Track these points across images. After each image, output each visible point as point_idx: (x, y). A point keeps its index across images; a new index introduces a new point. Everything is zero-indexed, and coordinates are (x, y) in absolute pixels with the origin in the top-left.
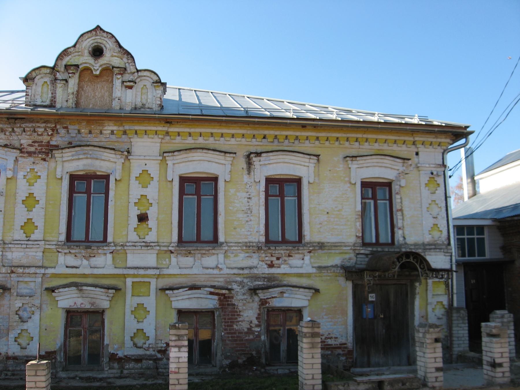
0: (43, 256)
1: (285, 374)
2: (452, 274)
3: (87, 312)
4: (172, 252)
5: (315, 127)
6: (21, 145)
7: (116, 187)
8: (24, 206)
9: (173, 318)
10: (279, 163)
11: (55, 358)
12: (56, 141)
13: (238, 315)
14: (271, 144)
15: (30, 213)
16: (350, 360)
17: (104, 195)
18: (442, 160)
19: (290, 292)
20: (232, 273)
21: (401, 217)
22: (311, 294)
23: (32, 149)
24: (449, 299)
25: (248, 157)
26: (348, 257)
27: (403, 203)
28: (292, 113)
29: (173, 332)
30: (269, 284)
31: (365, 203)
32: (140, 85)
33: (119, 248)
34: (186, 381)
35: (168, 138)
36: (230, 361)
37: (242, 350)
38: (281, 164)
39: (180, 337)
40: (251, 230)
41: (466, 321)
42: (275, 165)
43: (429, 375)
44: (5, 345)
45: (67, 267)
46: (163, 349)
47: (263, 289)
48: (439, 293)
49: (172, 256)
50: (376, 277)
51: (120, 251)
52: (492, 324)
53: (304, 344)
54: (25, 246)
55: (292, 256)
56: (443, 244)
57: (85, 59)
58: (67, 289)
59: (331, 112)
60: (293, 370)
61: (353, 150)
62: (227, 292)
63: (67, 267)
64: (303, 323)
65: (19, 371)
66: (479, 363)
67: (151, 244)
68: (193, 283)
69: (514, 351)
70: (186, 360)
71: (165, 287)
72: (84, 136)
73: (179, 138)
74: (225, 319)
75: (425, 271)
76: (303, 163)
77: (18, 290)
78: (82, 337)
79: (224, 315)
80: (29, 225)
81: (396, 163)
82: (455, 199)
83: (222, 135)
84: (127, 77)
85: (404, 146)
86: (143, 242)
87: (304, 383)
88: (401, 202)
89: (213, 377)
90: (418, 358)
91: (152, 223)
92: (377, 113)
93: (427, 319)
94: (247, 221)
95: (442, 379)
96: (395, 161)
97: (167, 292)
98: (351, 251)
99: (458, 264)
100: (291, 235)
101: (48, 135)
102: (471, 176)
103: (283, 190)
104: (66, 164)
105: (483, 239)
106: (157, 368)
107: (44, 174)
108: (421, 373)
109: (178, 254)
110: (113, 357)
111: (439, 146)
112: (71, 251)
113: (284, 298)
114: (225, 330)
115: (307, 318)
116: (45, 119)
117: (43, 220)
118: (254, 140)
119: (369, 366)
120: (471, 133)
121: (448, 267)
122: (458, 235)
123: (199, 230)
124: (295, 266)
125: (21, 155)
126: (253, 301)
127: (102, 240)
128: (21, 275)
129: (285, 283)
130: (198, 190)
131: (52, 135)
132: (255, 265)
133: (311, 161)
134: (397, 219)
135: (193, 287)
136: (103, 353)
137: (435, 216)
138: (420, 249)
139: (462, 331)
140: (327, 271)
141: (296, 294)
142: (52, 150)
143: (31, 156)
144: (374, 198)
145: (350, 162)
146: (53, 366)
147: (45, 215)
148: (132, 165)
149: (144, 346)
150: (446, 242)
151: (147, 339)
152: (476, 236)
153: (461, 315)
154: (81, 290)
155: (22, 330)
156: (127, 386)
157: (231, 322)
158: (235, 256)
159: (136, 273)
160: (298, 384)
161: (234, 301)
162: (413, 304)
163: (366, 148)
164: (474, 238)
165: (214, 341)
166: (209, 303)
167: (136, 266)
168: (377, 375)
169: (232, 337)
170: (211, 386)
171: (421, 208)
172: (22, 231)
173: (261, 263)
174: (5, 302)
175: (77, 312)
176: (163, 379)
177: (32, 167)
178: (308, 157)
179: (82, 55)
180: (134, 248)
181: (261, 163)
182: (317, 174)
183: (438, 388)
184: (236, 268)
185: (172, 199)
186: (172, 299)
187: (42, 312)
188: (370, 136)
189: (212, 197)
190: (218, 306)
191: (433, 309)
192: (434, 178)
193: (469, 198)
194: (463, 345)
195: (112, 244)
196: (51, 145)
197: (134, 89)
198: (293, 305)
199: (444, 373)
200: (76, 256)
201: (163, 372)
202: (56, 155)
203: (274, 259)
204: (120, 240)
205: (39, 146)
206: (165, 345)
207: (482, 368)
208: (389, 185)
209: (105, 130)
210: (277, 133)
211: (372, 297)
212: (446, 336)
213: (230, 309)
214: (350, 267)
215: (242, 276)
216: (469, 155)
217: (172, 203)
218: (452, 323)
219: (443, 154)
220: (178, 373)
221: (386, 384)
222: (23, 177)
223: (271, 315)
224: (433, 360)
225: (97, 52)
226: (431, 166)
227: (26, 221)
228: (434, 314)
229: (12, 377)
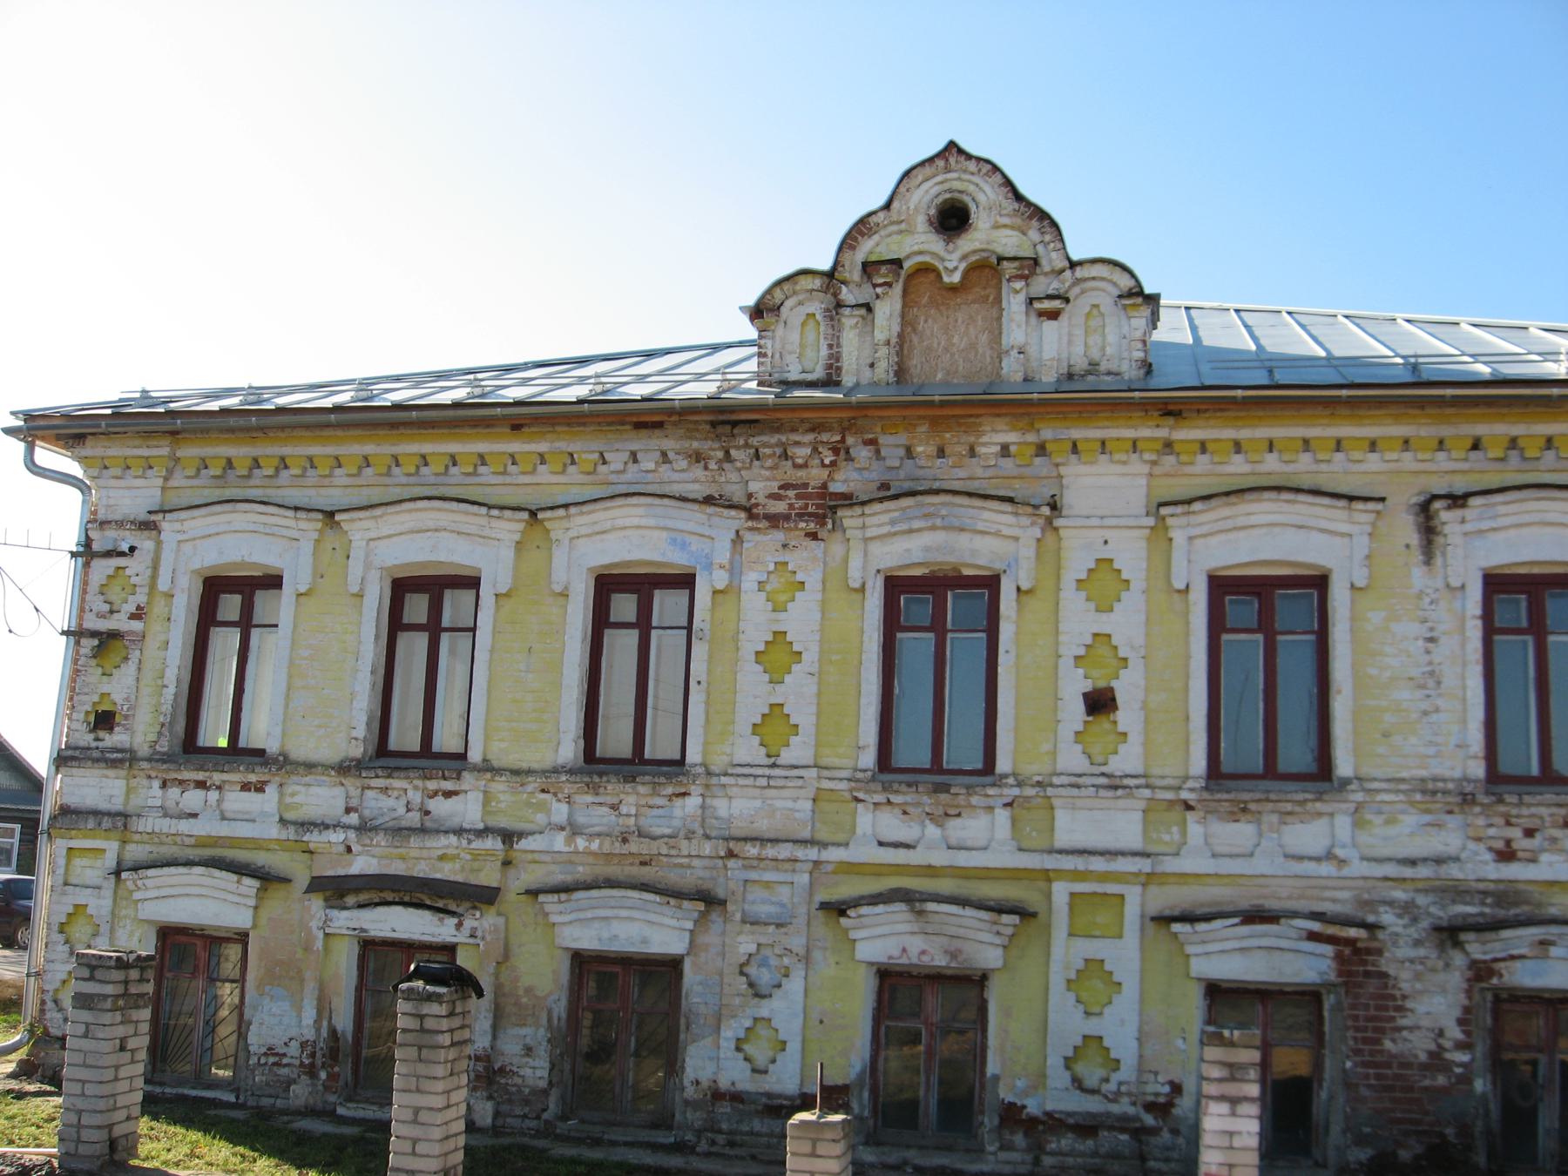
23: (780, 507)
30: (1501, 913)
49: (1190, 816)
51: (1033, 800)
57: (917, 241)
58: (880, 908)
84: (1041, 285)
91: (1127, 716)
97: (1177, 927)
104: (876, 549)
107: (813, 578)
110: (1011, 1115)
114: (1357, 1052)
116: (813, 419)
130: (1267, 614)
154: (921, 913)
161: (1386, 965)
181: (1468, 527)
186: (1190, 949)
197: (1064, 318)
203: (1516, 833)
204: (1034, 768)
210: (1517, 430)
217: (1188, 657)
225: (953, 218)
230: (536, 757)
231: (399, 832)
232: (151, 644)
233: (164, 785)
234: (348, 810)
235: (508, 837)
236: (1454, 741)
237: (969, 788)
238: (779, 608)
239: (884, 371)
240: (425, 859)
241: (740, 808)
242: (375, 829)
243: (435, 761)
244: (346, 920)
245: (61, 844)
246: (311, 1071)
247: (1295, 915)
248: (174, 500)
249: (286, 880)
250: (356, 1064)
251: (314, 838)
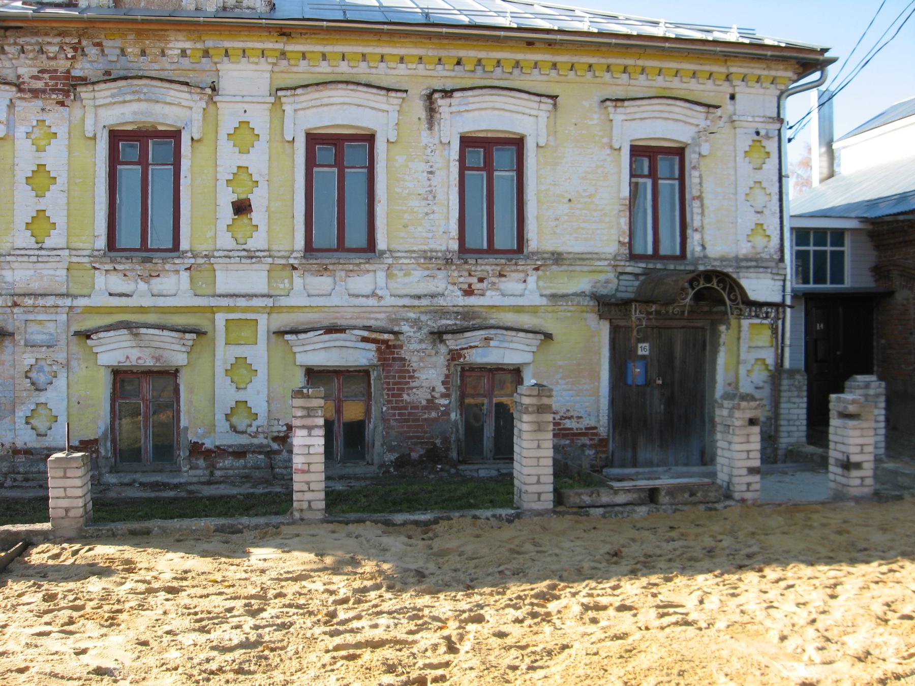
0: (67, 276)
1: (491, 477)
2: (784, 312)
3: (149, 373)
4: (294, 268)
5: (550, 44)
6: (19, 77)
7: (192, 152)
8: (30, 188)
9: (299, 380)
10: (486, 109)
11: (97, 451)
12: (81, 69)
13: (411, 377)
14: (471, 75)
15: (41, 199)
16: (603, 456)
17: (171, 167)
18: (776, 110)
19: (501, 338)
20: (401, 304)
22: (538, 342)
23: (40, 85)
24: (777, 354)
25: (429, 97)
26: (604, 279)
27: (704, 185)
28: (510, 19)
29: (299, 402)
31: (637, 184)
33: (201, 261)
34: (322, 486)
35: (285, 62)
36: (397, 455)
37: (418, 437)
38: (489, 112)
39: (310, 412)
40: (434, 229)
41: (805, 394)
42: (476, 113)
43: (736, 480)
44: (10, 430)
45: (111, 295)
46: (282, 434)
47: (454, 332)
48: (761, 344)
49: (295, 274)
50: (651, 313)
51: (202, 266)
52: (847, 396)
53: (524, 425)
54: (34, 259)
55: (505, 276)
56: (771, 259)
58: (112, 333)
59: (580, 19)
60: (504, 471)
61: (618, 88)
62: (391, 337)
63: (111, 295)
64: (522, 389)
65: (36, 473)
66: (823, 463)
67: (257, 254)
68: (332, 321)
69: (883, 445)
70: (322, 450)
71: (282, 329)
72: (132, 59)
73: (305, 62)
74: (388, 383)
75: (738, 304)
76: (528, 111)
77: (27, 336)
78: (141, 418)
79: (386, 377)
80: (40, 221)
81: (694, 113)
82: (797, 184)
83: (382, 58)
85: (710, 82)
86: (244, 250)
87: (523, 490)
88: (700, 184)
89: (368, 482)
90: (719, 452)
91: (258, 215)
92: (662, 21)
93: (737, 388)
94: (427, 214)
95: (757, 486)
96: (691, 109)
97: (288, 337)
98: (609, 268)
99: (796, 296)
100: (505, 239)
101: (67, 58)
102: (828, 144)
103: (490, 157)
104: (102, 112)
105: (842, 252)
106: (272, 468)
107: (62, 131)
108: (722, 478)
109: (304, 271)
110: (196, 449)
111: (772, 83)
112: (117, 267)
113: (490, 349)
114: (389, 402)
115: (529, 380)
117: (65, 213)
118: (440, 67)
119: (634, 464)
120: (832, 61)
121: (777, 299)
122: (797, 245)
123: (341, 231)
124: (510, 293)
125: (19, 95)
126: (437, 353)
127: (170, 246)
128: (31, 309)
129: (492, 322)
130: (339, 156)
131: (73, 57)
132: (440, 290)
133: (543, 106)
134: (692, 213)
135: (332, 329)
136: (178, 444)
137: (760, 210)
138: (731, 266)
139: (796, 410)
140: (567, 302)
141: (511, 342)
142: (74, 87)
143: (37, 97)
144: (653, 174)
145: (611, 110)
146: (93, 464)
147: (68, 203)
148: (220, 112)
149: (249, 430)
150: (776, 257)
151: (254, 417)
152: (829, 248)
153: (796, 383)
154: (137, 335)
155: (37, 404)
156: (221, 497)
157: (399, 389)
158: (405, 275)
159: (231, 305)
160: (513, 494)
161: (403, 353)
163: (642, 84)
164: (825, 252)
165: (370, 422)
166: (360, 355)
167: (232, 291)
168: (649, 479)
169: (399, 414)
170: (364, 496)
171: (736, 194)
172: (29, 233)
173: (450, 287)
174: (7, 357)
175: (132, 372)
176: (283, 485)
177: (41, 118)
178: (537, 99)
180: (228, 260)
181: (453, 109)
182: (553, 131)
183: (750, 502)
184: (407, 296)
185: (293, 173)
186: (295, 349)
187: (70, 374)
189: (365, 170)
190: (375, 361)
192: (760, 141)
193: (822, 181)
194: (796, 434)
195: (189, 254)
196: (73, 77)
198: (506, 361)
199: (762, 478)
200: (125, 275)
201: (282, 474)
202: (83, 95)
203: (474, 280)
204: (203, 247)
205: (51, 78)
206: (285, 428)
207: (827, 471)
208: (680, 152)
209: (171, 49)
210: (482, 55)
211: (643, 349)
212: (769, 418)
213: (397, 366)
214: (607, 296)
215: (417, 310)
216: (825, 102)
217: (294, 181)
218: (779, 397)
219: (779, 98)
220: (308, 472)
221: (663, 493)
222: (24, 135)
223: (469, 377)
224: (744, 455)
226: (757, 119)
227: (35, 169)
228: (749, 380)
229: (24, 484)
247: (355, 328)
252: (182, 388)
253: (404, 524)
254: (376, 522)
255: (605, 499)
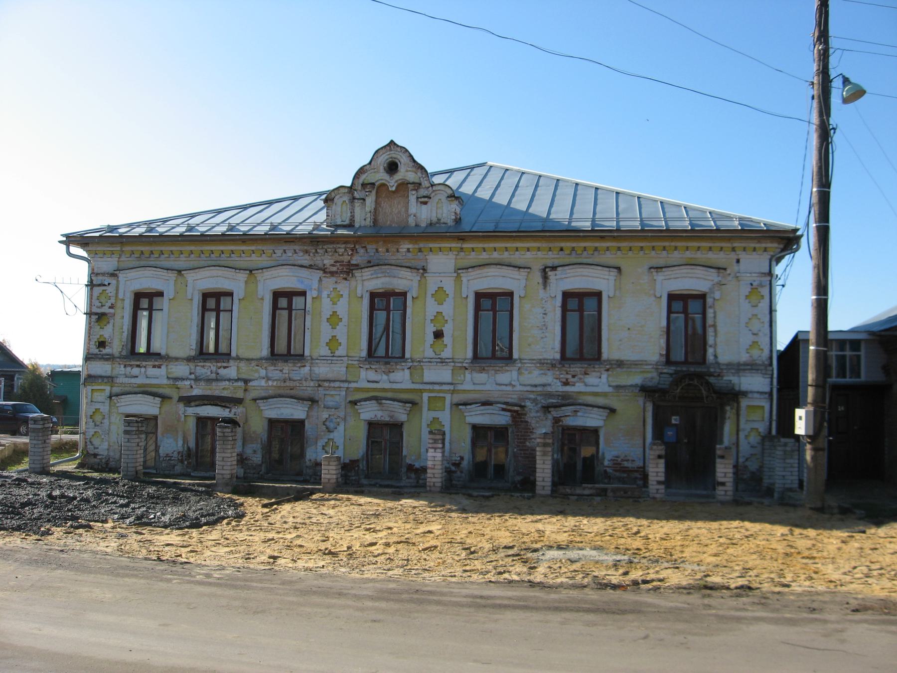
21: (713, 334)
22: (606, 414)
23: (334, 269)
26: (649, 376)
30: (564, 402)
32: (434, 200)
33: (416, 364)
49: (467, 372)
51: (416, 367)
56: (763, 364)
57: (380, 176)
58: (368, 402)
80: (333, 342)
84: (423, 192)
91: (447, 339)
97: (461, 407)
104: (366, 283)
107: (346, 293)
110: (410, 468)
114: (518, 446)
116: (345, 239)
129: (580, 401)
130: (492, 305)
133: (612, 273)
145: (654, 273)
154: (381, 404)
161: (527, 418)
162: (722, 429)
166: (501, 419)
179: (378, 172)
181: (557, 277)
186: (466, 414)
188: (679, 244)
190: (510, 422)
191: (746, 437)
197: (429, 204)
203: (569, 376)
204: (417, 356)
208: (702, 297)
210: (574, 245)
211: (675, 420)
217: (467, 319)
225: (392, 167)
230: (256, 354)
231: (209, 381)
232: (118, 317)
233: (125, 366)
234: (191, 374)
235: (246, 381)
236: (551, 348)
237: (396, 363)
238: (334, 304)
239: (369, 222)
240: (217, 390)
241: (322, 370)
242: (200, 380)
243: (222, 356)
244: (191, 411)
245: (89, 388)
246: (182, 461)
248: (122, 265)
249: (170, 398)
250: (197, 457)
251: (179, 383)
252: (404, 434)
253: (477, 497)
254: (464, 494)
255: (578, 491)
